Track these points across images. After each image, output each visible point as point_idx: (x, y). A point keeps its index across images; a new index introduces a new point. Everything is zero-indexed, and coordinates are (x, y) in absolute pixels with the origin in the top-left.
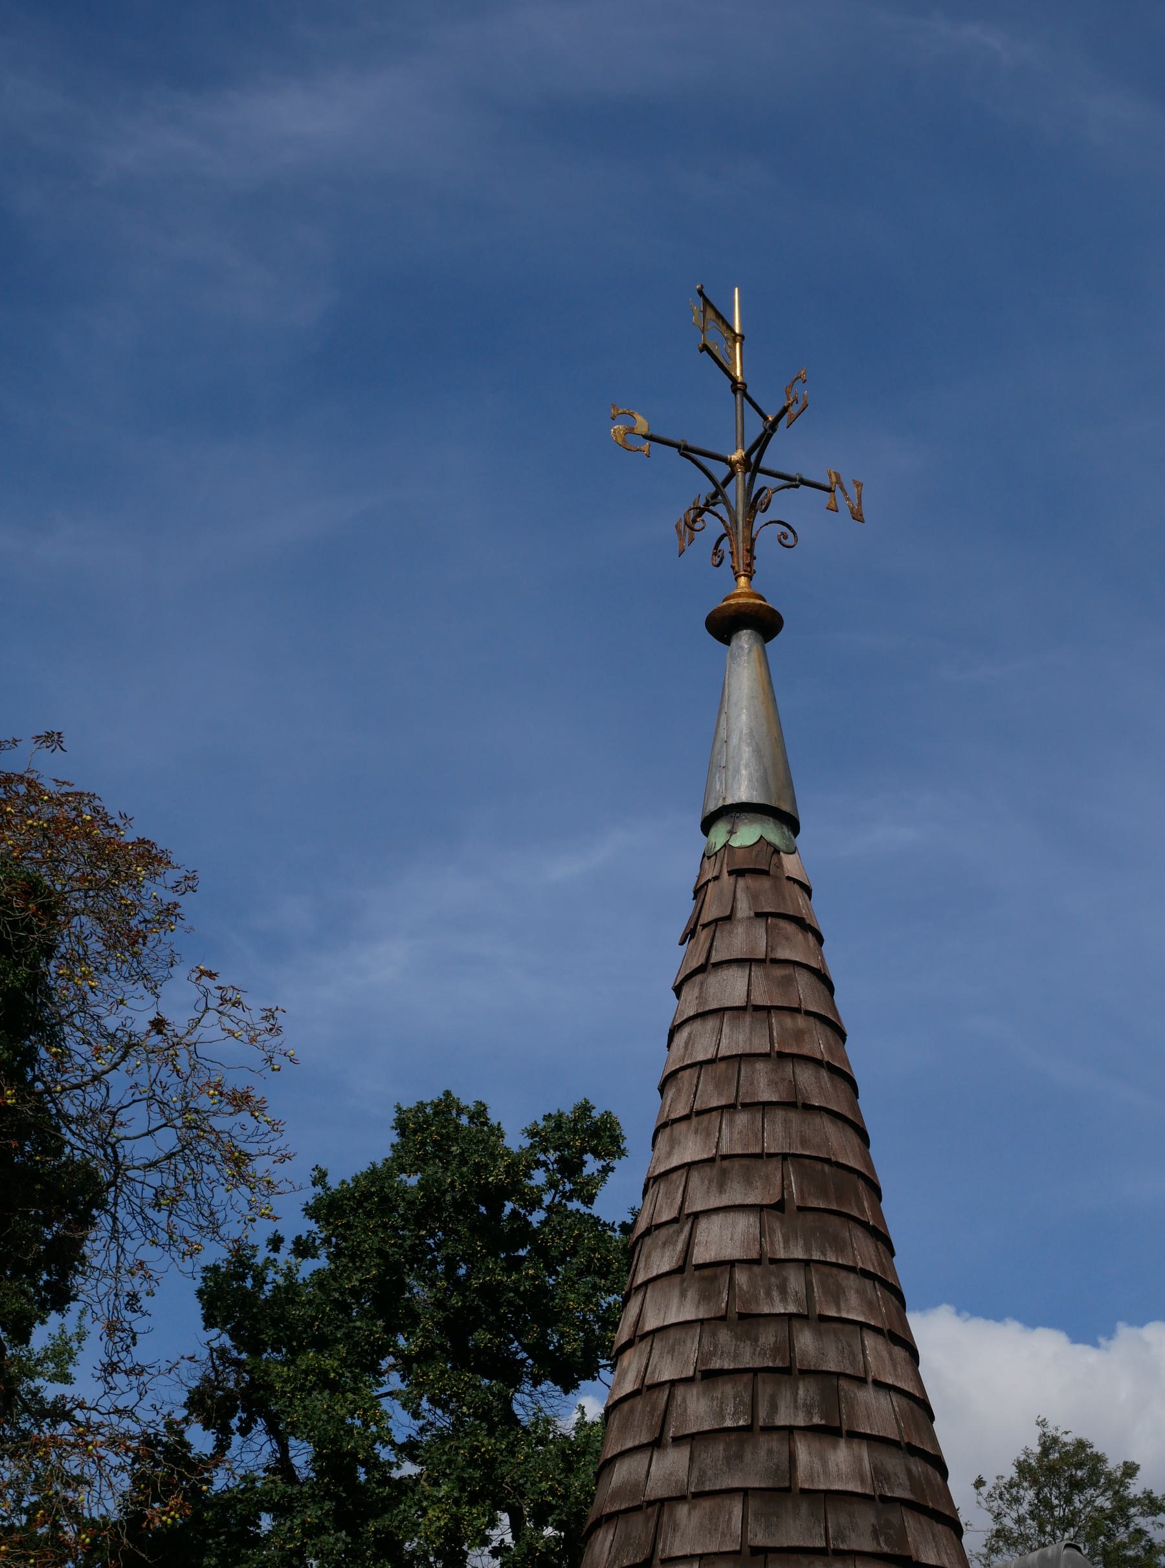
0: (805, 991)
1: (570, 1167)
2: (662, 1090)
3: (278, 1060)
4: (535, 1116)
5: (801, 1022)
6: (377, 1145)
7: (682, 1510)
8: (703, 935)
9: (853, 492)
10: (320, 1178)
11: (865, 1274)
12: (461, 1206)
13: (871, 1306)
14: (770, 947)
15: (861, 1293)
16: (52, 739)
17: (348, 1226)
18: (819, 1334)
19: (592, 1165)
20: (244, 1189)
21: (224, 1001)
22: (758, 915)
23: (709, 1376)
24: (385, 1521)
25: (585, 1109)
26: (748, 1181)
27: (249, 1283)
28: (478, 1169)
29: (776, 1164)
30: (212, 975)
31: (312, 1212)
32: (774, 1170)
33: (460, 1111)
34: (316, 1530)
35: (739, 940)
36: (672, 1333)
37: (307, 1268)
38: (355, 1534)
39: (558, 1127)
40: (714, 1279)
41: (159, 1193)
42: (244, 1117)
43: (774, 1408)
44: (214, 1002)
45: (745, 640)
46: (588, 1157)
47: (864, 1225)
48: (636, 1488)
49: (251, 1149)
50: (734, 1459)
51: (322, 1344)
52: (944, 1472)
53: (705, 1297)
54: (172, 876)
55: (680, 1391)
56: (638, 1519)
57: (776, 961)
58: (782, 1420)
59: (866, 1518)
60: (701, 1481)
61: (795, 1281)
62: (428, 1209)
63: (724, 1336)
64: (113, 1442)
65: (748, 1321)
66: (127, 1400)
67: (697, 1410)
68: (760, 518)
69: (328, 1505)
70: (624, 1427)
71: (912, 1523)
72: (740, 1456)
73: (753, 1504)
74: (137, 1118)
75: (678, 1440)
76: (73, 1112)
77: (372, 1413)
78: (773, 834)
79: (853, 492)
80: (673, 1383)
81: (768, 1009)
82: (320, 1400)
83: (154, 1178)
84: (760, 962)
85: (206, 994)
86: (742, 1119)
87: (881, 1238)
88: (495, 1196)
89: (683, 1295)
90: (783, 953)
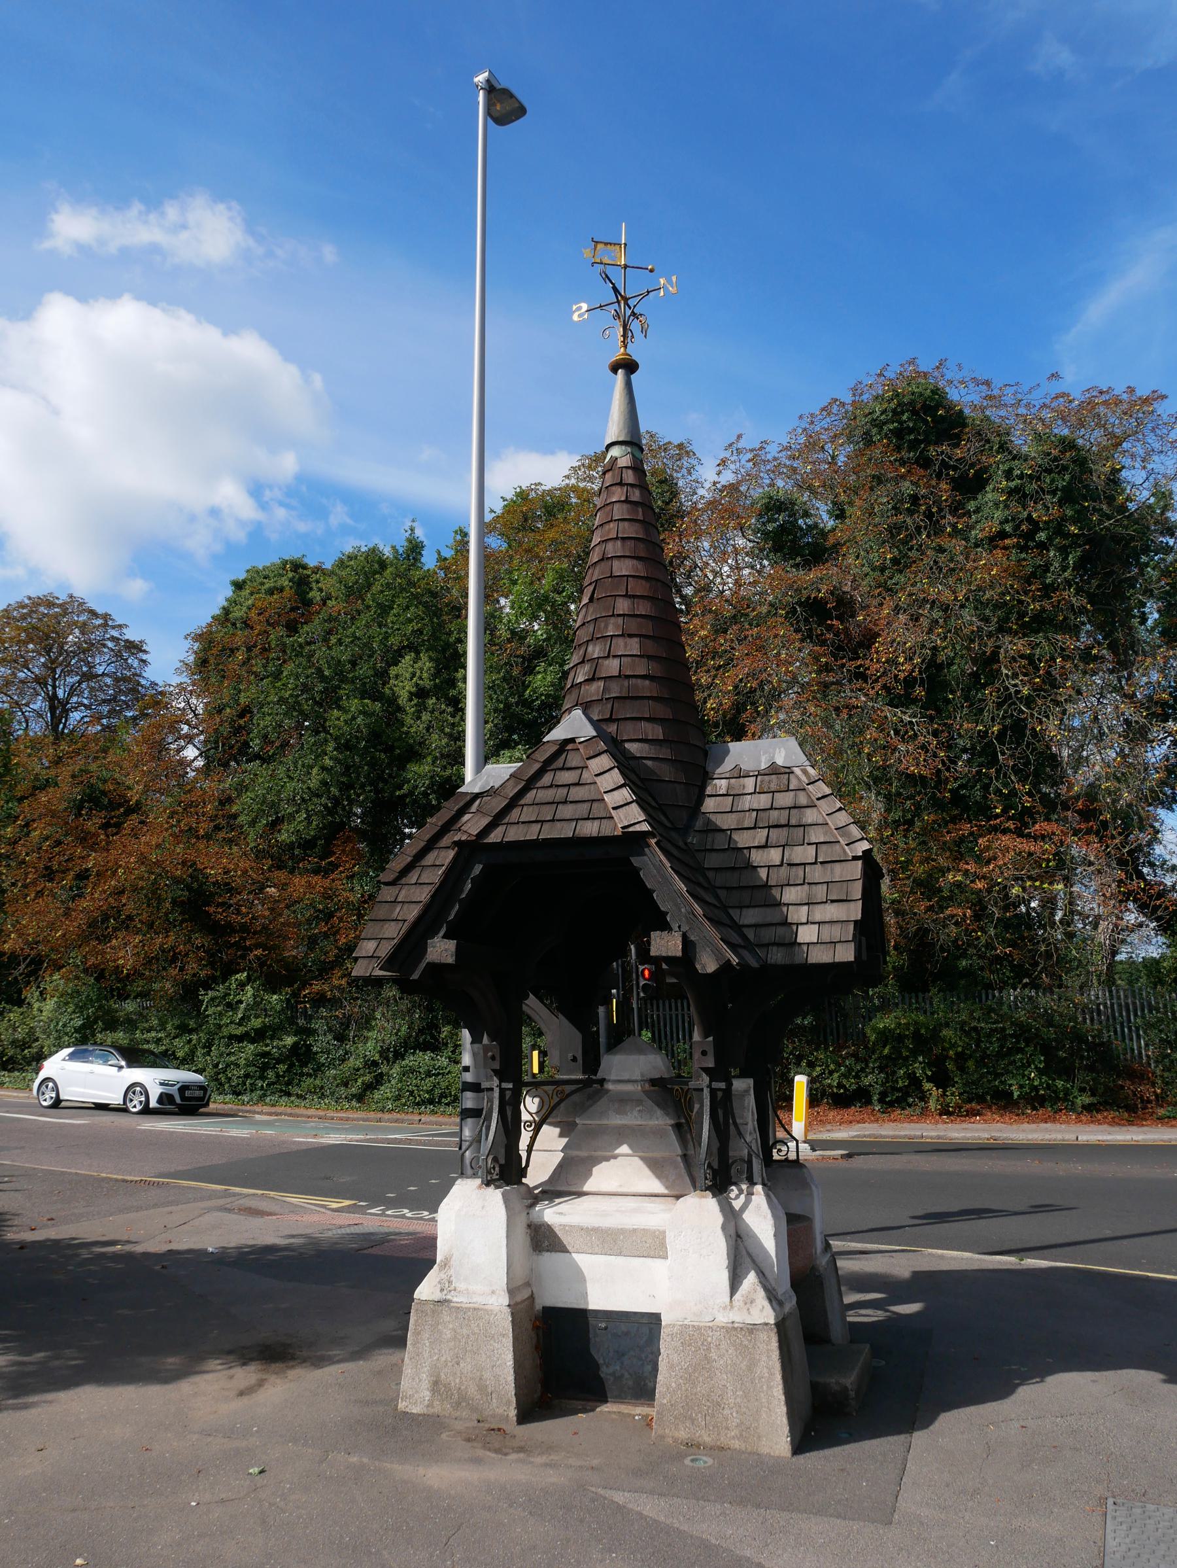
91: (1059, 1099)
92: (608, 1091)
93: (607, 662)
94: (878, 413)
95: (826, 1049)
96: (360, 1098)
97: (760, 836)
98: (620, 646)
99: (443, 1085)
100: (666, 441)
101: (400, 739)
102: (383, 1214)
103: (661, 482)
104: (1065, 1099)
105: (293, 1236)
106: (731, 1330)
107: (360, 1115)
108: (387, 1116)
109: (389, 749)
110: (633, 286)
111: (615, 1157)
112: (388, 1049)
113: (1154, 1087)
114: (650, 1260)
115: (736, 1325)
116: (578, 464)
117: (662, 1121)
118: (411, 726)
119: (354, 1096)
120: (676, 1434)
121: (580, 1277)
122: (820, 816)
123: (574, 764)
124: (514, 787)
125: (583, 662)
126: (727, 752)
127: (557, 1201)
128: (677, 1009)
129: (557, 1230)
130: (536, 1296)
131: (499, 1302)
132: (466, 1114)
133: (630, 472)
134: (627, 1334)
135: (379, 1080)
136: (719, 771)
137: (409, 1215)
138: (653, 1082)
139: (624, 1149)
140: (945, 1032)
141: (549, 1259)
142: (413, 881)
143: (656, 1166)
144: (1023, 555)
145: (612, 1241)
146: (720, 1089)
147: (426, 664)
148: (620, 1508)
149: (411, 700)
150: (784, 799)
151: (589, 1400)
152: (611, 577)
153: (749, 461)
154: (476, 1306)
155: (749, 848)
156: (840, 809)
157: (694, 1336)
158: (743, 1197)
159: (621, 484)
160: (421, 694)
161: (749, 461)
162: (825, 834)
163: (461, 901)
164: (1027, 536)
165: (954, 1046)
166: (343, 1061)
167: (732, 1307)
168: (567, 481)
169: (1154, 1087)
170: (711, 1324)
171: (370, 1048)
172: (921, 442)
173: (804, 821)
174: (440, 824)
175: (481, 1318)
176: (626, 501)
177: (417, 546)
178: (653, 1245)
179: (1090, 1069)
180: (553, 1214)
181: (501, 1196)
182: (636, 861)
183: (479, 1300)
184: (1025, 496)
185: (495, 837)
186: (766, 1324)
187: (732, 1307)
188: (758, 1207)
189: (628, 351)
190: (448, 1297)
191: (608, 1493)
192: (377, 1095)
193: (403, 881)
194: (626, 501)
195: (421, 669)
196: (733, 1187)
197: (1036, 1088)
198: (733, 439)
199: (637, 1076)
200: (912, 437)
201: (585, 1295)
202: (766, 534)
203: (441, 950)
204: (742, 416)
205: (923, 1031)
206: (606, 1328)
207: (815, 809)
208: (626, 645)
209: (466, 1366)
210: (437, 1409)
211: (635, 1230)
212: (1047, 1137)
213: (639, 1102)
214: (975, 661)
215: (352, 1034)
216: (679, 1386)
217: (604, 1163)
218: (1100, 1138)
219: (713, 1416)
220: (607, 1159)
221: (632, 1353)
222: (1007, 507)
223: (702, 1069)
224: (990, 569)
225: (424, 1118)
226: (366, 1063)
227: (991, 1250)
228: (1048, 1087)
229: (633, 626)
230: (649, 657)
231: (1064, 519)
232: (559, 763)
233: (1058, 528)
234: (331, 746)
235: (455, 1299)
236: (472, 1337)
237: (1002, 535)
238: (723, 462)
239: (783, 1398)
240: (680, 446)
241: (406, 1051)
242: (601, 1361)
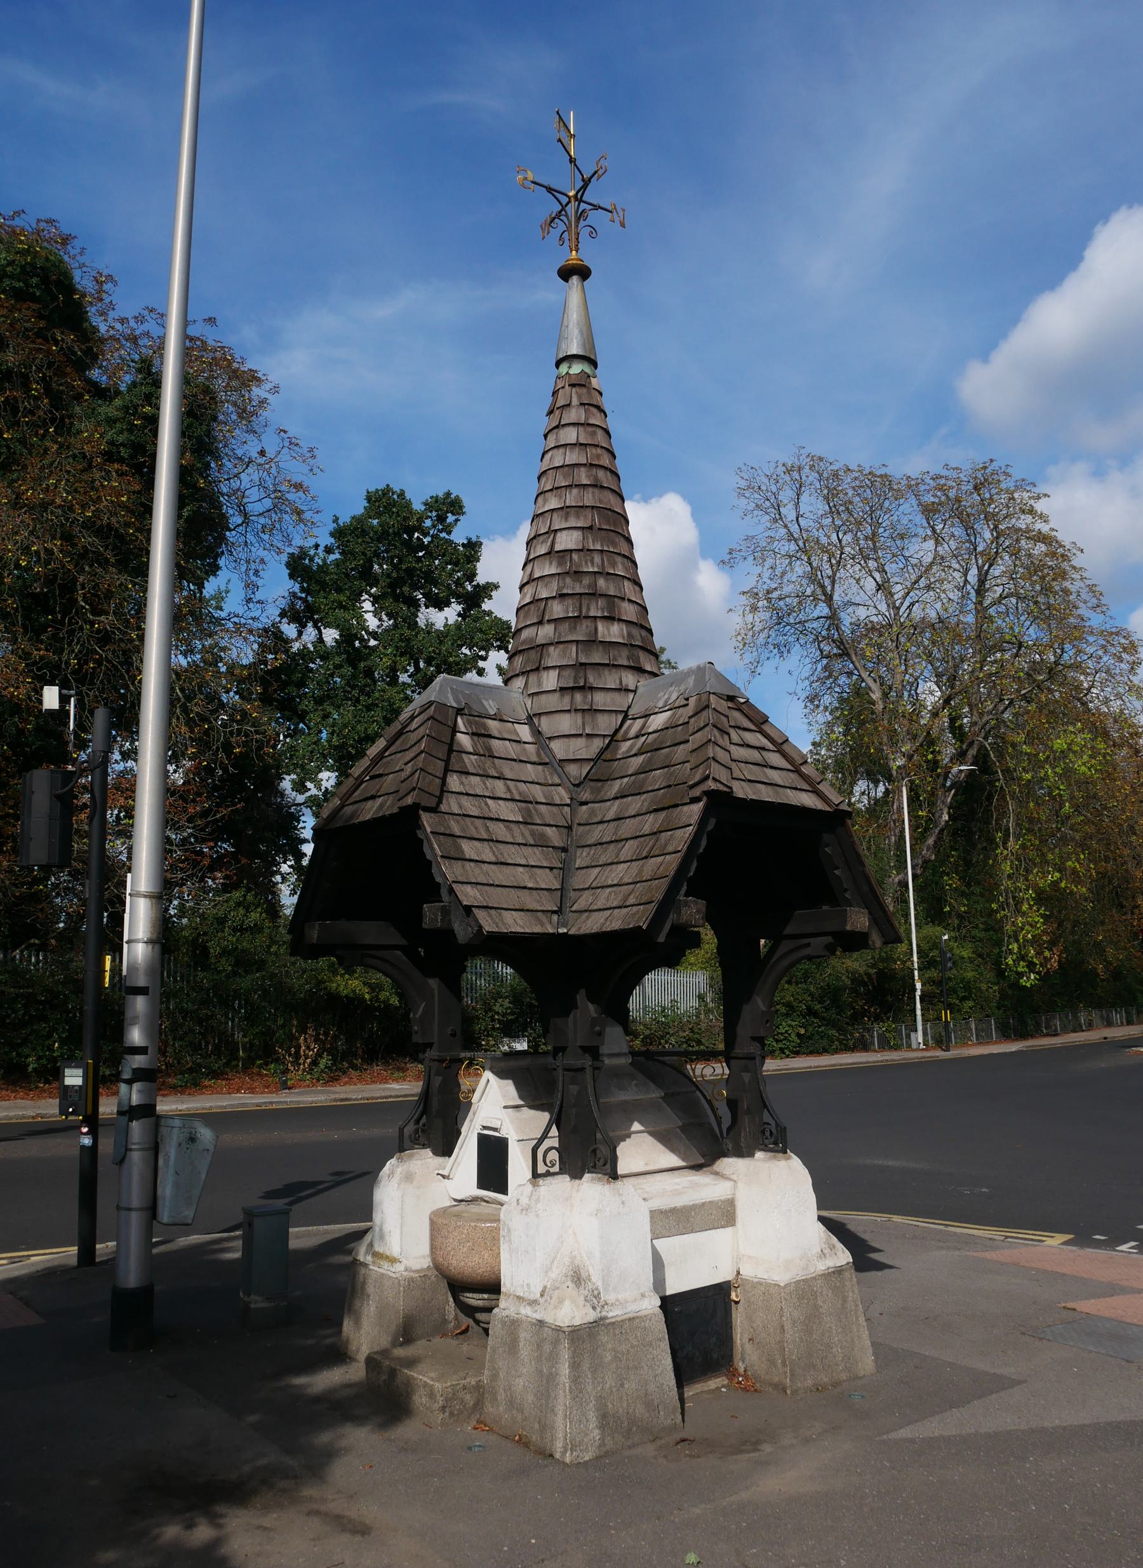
0: (600, 437)
1: (441, 519)
2: (539, 479)
3: (315, 470)
4: (426, 497)
5: (599, 451)
6: (359, 507)
7: (552, 649)
8: (557, 412)
9: (621, 213)
10: (336, 520)
11: (624, 556)
12: (398, 534)
13: (626, 569)
14: (587, 418)
15: (623, 564)
16: (211, 321)
17: (348, 541)
18: (606, 580)
19: (451, 518)
20: (302, 525)
21: (291, 443)
22: (581, 404)
23: (562, 596)
24: (368, 663)
25: (448, 494)
26: (578, 517)
27: (307, 561)
28: (405, 519)
29: (589, 510)
30: (285, 432)
31: (332, 535)
32: (588, 512)
33: (393, 493)
34: (338, 667)
35: (573, 415)
36: (546, 579)
37: (332, 557)
38: (355, 667)
39: (436, 501)
40: (563, 557)
41: (264, 526)
42: (301, 494)
43: (588, 609)
44: (287, 444)
45: (575, 280)
46: (449, 515)
47: (624, 536)
48: (532, 640)
49: (304, 508)
50: (573, 629)
51: (339, 590)
52: (652, 635)
53: (560, 564)
54: (268, 386)
55: (550, 602)
56: (533, 652)
57: (588, 424)
58: (592, 614)
59: (625, 652)
60: (559, 637)
61: (597, 558)
62: (383, 535)
63: (568, 580)
64: (250, 631)
65: (578, 574)
66: (257, 614)
67: (557, 609)
68: (582, 223)
69: (344, 656)
70: (526, 617)
71: (642, 655)
72: (575, 628)
73: (580, 647)
74: (254, 494)
75: (549, 621)
76: (225, 490)
77: (360, 619)
78: (587, 368)
79: (621, 213)
80: (547, 599)
81: (586, 445)
82: (339, 613)
83: (262, 520)
84: (582, 424)
85: (283, 439)
86: (575, 491)
87: (629, 541)
88: (410, 531)
89: (551, 563)
90: (592, 421)
143: (664, 1138)
154: (631, 1315)
178: (724, 1214)
190: (604, 1314)
209: (630, 1386)
211: (703, 1204)
235: (610, 1314)
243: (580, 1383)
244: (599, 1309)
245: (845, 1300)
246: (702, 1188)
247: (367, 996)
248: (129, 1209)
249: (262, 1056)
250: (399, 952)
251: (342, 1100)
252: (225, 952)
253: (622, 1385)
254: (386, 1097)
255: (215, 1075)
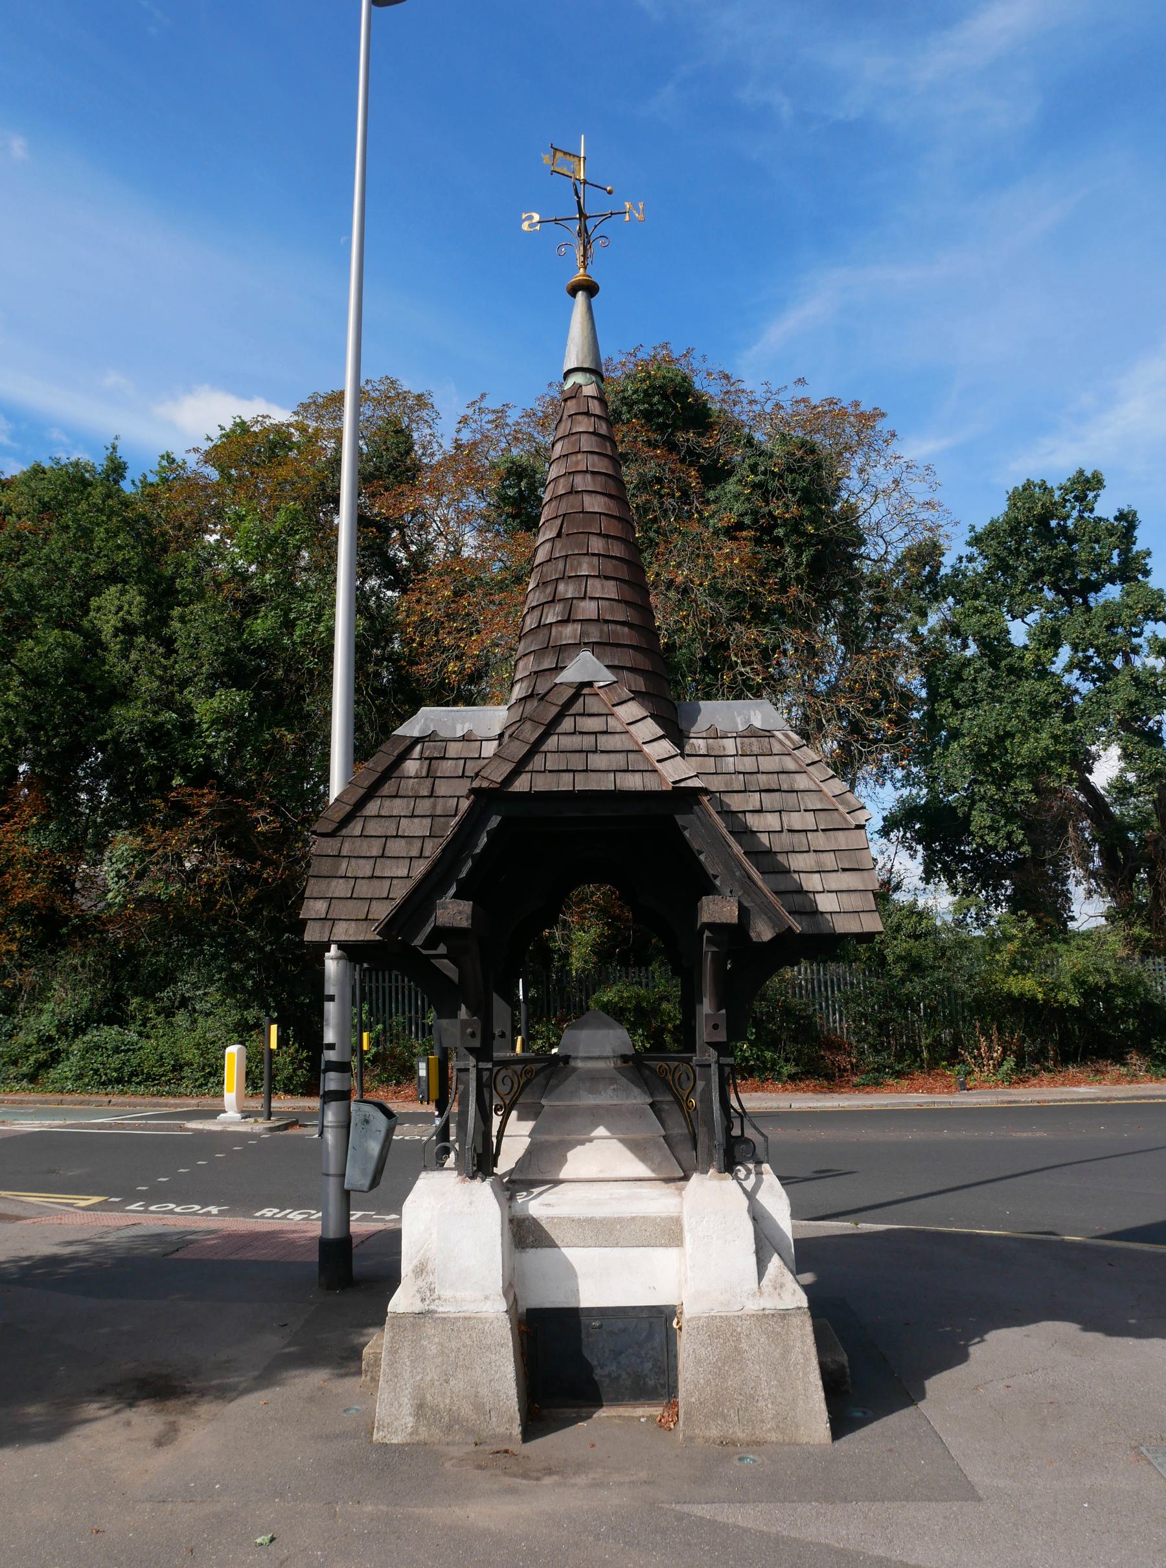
38: (996, 667)
45: (580, 295)
91: (767, 1069)
92: (575, 1069)
93: (583, 604)
94: (630, 392)
95: (549, 1021)
96: (33, 1078)
97: (754, 800)
98: (596, 588)
99: (135, 1062)
100: (405, 389)
101: (101, 677)
102: (146, 1211)
103: (397, 432)
104: (772, 1069)
105: (70, 1243)
106: (762, 1317)
107: (33, 1097)
108: (68, 1097)
109: (89, 689)
110: (594, 204)
111: (591, 1140)
112: (67, 1023)
113: (849, 1056)
114: (650, 1249)
115: (767, 1312)
116: (307, 401)
117: (639, 1099)
118: (114, 666)
119: (24, 1076)
120: (708, 1434)
121: (570, 1273)
122: (811, 783)
123: (595, 710)
124: (533, 731)
125: (553, 601)
126: (699, 710)
127: (536, 1191)
128: (377, 981)
129: (543, 1223)
130: (519, 1298)
131: (495, 1309)
132: (329, 1097)
133: (596, 402)
134: (625, 1330)
135: (55, 1058)
136: (693, 729)
137: (178, 1210)
138: (625, 1058)
139: (601, 1131)
140: (664, 1005)
141: (535, 1257)
142: (358, 833)
143: (637, 1148)
144: (758, 549)
145: (606, 1232)
146: (728, 1065)
147: (135, 599)
148: (712, 1523)
149: (116, 636)
150: (767, 763)
151: (581, 1407)
152: (582, 512)
153: (489, 422)
154: (467, 1315)
155: (744, 812)
156: (833, 777)
157: (722, 1328)
158: (753, 1177)
159: (587, 414)
160: (127, 630)
161: (489, 422)
162: (821, 800)
163: (473, 857)
164: (767, 532)
165: (671, 1019)
166: (11, 1036)
167: (761, 1293)
168: (296, 418)
169: (849, 1056)
170: (740, 1313)
171: (45, 1021)
172: (669, 426)
173: (796, 787)
174: (380, 769)
175: (473, 1328)
176: (594, 433)
177: (120, 467)
178: (669, 1233)
179: (794, 1040)
180: (539, 1206)
181: (490, 1190)
182: (680, 820)
183: (470, 1308)
184: (767, 491)
185: (521, 785)
186: (799, 1308)
187: (761, 1293)
188: (771, 1186)
189: (588, 272)
190: (432, 1307)
191: (686, 1508)
192: (53, 1074)
193: (344, 832)
194: (594, 433)
195: (130, 604)
196: (739, 1167)
197: (747, 1059)
198: (477, 397)
199: (608, 1052)
200: (661, 420)
201: (576, 1293)
202: (504, 498)
203: (454, 911)
204: (494, 372)
205: (645, 1004)
206: (600, 1327)
207: (804, 775)
208: (603, 587)
210: (423, 1434)
211: (633, 1218)
212: (764, 1105)
213: (612, 1080)
214: (706, 646)
215: (22, 1005)
216: (708, 1382)
217: (579, 1148)
218: (811, 1105)
219: (746, 1410)
220: (582, 1143)
221: (631, 1351)
222: (748, 499)
223: (709, 1044)
224: (732, 559)
225: (114, 1099)
226: (40, 1038)
227: (810, 1216)
228: (758, 1059)
229: (609, 567)
230: (627, 603)
231: (801, 517)
232: (577, 707)
233: (795, 526)
234: (17, 679)
235: (440, 1309)
236: (464, 1351)
237: (740, 526)
238: (464, 420)
239: (820, 1383)
240: (419, 397)
241: (88, 1025)
242: (595, 1363)
243: (396, 1369)
244: (428, 1302)
245: (786, 1351)
246: (657, 1201)
247: (1040, 996)
248: (328, 1175)
249: (945, 1057)
250: (446, 961)
251: (1010, 1102)
252: (899, 959)
253: (447, 1382)
254: (1060, 1101)
255: (899, 1075)
